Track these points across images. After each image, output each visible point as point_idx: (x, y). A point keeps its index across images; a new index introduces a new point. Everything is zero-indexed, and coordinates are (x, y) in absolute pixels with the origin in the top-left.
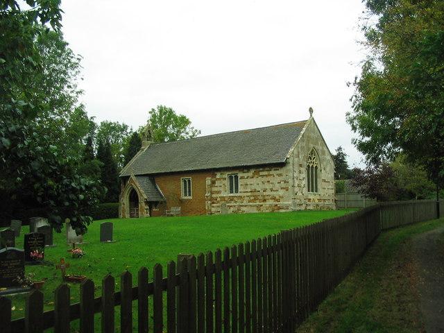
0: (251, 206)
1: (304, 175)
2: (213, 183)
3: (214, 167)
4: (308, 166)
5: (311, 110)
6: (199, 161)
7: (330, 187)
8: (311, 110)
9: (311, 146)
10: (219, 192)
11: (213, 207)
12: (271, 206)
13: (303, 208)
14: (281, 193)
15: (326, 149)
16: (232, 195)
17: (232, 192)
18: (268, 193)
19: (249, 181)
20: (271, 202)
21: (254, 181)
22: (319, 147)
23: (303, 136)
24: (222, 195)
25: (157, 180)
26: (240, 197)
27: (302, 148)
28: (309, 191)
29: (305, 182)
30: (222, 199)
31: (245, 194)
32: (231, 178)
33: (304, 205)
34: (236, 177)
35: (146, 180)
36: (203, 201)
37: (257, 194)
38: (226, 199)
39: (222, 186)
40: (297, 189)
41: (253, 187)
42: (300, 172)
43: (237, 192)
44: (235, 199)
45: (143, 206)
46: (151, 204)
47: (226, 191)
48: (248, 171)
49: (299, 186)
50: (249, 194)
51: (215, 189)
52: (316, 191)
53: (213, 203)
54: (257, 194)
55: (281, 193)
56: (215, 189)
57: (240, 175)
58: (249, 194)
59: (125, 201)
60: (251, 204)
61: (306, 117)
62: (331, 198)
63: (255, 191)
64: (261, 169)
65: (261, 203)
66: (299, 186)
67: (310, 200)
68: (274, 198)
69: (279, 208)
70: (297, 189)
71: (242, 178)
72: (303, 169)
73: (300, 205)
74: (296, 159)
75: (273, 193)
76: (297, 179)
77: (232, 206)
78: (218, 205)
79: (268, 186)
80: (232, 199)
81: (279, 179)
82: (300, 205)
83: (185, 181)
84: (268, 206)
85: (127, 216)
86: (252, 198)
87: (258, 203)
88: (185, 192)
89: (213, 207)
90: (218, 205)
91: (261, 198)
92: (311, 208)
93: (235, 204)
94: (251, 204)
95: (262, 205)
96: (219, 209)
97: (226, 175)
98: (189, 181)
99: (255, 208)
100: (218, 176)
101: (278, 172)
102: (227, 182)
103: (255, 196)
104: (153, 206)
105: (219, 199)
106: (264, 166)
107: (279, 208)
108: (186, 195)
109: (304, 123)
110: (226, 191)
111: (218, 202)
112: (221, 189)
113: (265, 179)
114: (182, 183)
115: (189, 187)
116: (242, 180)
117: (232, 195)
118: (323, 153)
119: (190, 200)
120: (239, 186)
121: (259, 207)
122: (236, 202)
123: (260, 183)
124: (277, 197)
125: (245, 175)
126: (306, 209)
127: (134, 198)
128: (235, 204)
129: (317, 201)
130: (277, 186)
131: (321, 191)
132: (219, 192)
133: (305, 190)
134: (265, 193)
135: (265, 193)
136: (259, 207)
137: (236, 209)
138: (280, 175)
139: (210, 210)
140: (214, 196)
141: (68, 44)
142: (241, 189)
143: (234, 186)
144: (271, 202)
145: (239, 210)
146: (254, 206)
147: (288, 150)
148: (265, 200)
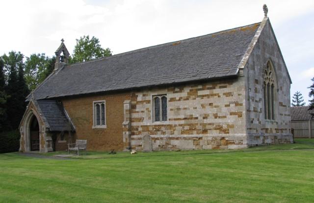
0: (185, 138)
1: (260, 95)
2: (133, 107)
3: (134, 86)
4: (265, 82)
5: (265, 9)
6: (115, 80)
7: (287, 113)
8: (265, 9)
9: (267, 56)
10: (141, 120)
11: (133, 139)
12: (214, 139)
13: (260, 142)
14: (231, 120)
15: (281, 63)
16: (158, 123)
17: (157, 119)
18: (211, 120)
19: (182, 104)
20: (216, 134)
21: (190, 103)
22: (276, 60)
23: (258, 40)
24: (145, 123)
25: (66, 104)
26: (170, 126)
27: (258, 56)
28: (266, 118)
29: (261, 105)
30: (146, 128)
31: (177, 123)
32: (156, 100)
33: (262, 138)
34: (164, 99)
35: (51, 105)
36: (120, 131)
37: (193, 121)
38: (151, 129)
39: (145, 105)
40: (253, 115)
41: (188, 113)
42: (256, 91)
43: (165, 118)
44: (163, 129)
45: (44, 137)
46: (54, 134)
47: (149, 118)
48: (181, 91)
49: (255, 111)
50: (183, 122)
51: (135, 115)
52: (273, 119)
53: (133, 134)
54: (193, 121)
55: (231, 120)
56: (135, 115)
57: (169, 96)
58: (183, 122)
59: (24, 129)
60: (185, 136)
61: (259, 18)
62: (288, 127)
63: (191, 118)
64: (200, 87)
65: (201, 135)
66: (255, 111)
67: (267, 129)
68: (219, 128)
69: (228, 143)
70: (253, 115)
71: (172, 100)
72: (259, 87)
73: (258, 137)
74: (251, 72)
75: (218, 121)
76: (253, 100)
77: (157, 139)
78: (139, 136)
79: (210, 111)
80: (157, 129)
81: (227, 100)
82: (258, 137)
83: (98, 106)
84: (210, 139)
85: (27, 149)
86: (187, 128)
87: (195, 135)
88: (98, 119)
89: (133, 139)
90: (139, 136)
91: (199, 127)
92: (268, 141)
93: (162, 136)
94: (185, 136)
95: (200, 138)
96: (141, 143)
97: (150, 96)
98: (103, 105)
99: (191, 142)
100: (140, 97)
101: (226, 90)
102: (151, 106)
103: (191, 125)
104: (59, 137)
105: (140, 129)
106: (203, 82)
107: (228, 143)
108: (99, 124)
109: (257, 25)
110: (149, 118)
111: (140, 133)
112: (144, 115)
113: (205, 101)
114: (94, 108)
115: (103, 114)
116: (172, 103)
117: (158, 123)
118: (280, 69)
119: (103, 130)
120: (168, 111)
121: (197, 140)
122: (164, 133)
123: (199, 106)
124: (225, 127)
125: (177, 96)
126: (264, 143)
127: (34, 127)
128: (162, 136)
129: (274, 132)
130: (224, 110)
131: (278, 118)
132: (141, 120)
133: (262, 116)
134: (205, 121)
135: (205, 121)
136: (197, 140)
137: (163, 143)
138: (228, 94)
139: (130, 144)
140: (134, 124)
141: (63, 48)
142: (170, 114)
143: (160, 112)
144: (216, 134)
145: (167, 144)
146: (190, 139)
147: (239, 58)
148: (205, 131)
